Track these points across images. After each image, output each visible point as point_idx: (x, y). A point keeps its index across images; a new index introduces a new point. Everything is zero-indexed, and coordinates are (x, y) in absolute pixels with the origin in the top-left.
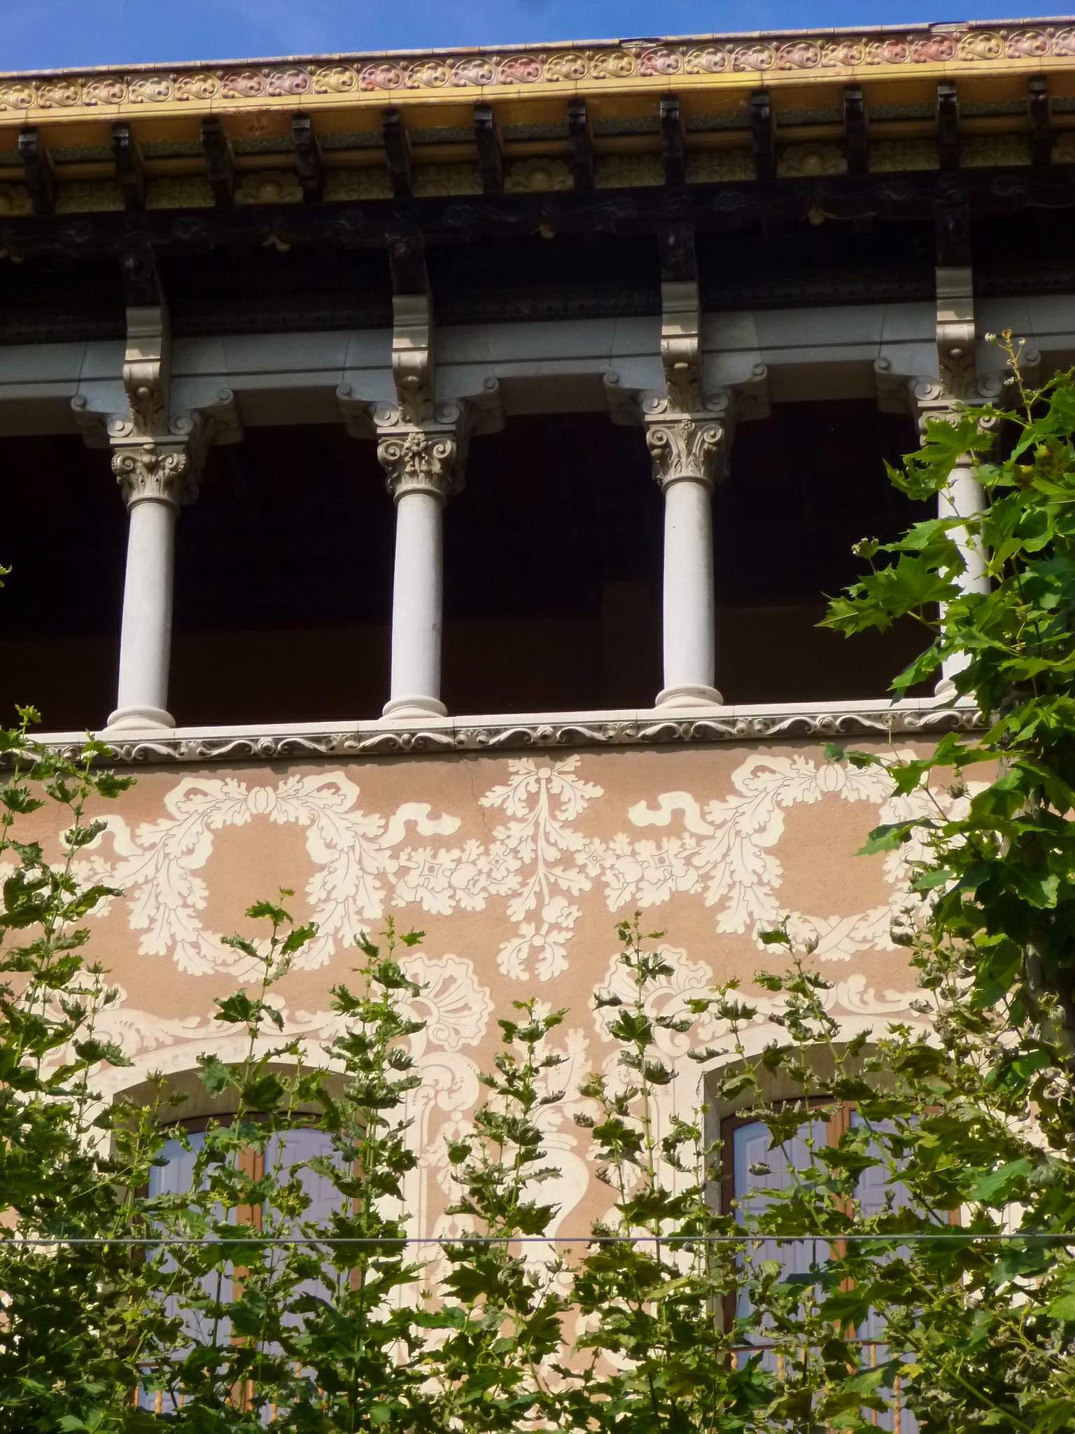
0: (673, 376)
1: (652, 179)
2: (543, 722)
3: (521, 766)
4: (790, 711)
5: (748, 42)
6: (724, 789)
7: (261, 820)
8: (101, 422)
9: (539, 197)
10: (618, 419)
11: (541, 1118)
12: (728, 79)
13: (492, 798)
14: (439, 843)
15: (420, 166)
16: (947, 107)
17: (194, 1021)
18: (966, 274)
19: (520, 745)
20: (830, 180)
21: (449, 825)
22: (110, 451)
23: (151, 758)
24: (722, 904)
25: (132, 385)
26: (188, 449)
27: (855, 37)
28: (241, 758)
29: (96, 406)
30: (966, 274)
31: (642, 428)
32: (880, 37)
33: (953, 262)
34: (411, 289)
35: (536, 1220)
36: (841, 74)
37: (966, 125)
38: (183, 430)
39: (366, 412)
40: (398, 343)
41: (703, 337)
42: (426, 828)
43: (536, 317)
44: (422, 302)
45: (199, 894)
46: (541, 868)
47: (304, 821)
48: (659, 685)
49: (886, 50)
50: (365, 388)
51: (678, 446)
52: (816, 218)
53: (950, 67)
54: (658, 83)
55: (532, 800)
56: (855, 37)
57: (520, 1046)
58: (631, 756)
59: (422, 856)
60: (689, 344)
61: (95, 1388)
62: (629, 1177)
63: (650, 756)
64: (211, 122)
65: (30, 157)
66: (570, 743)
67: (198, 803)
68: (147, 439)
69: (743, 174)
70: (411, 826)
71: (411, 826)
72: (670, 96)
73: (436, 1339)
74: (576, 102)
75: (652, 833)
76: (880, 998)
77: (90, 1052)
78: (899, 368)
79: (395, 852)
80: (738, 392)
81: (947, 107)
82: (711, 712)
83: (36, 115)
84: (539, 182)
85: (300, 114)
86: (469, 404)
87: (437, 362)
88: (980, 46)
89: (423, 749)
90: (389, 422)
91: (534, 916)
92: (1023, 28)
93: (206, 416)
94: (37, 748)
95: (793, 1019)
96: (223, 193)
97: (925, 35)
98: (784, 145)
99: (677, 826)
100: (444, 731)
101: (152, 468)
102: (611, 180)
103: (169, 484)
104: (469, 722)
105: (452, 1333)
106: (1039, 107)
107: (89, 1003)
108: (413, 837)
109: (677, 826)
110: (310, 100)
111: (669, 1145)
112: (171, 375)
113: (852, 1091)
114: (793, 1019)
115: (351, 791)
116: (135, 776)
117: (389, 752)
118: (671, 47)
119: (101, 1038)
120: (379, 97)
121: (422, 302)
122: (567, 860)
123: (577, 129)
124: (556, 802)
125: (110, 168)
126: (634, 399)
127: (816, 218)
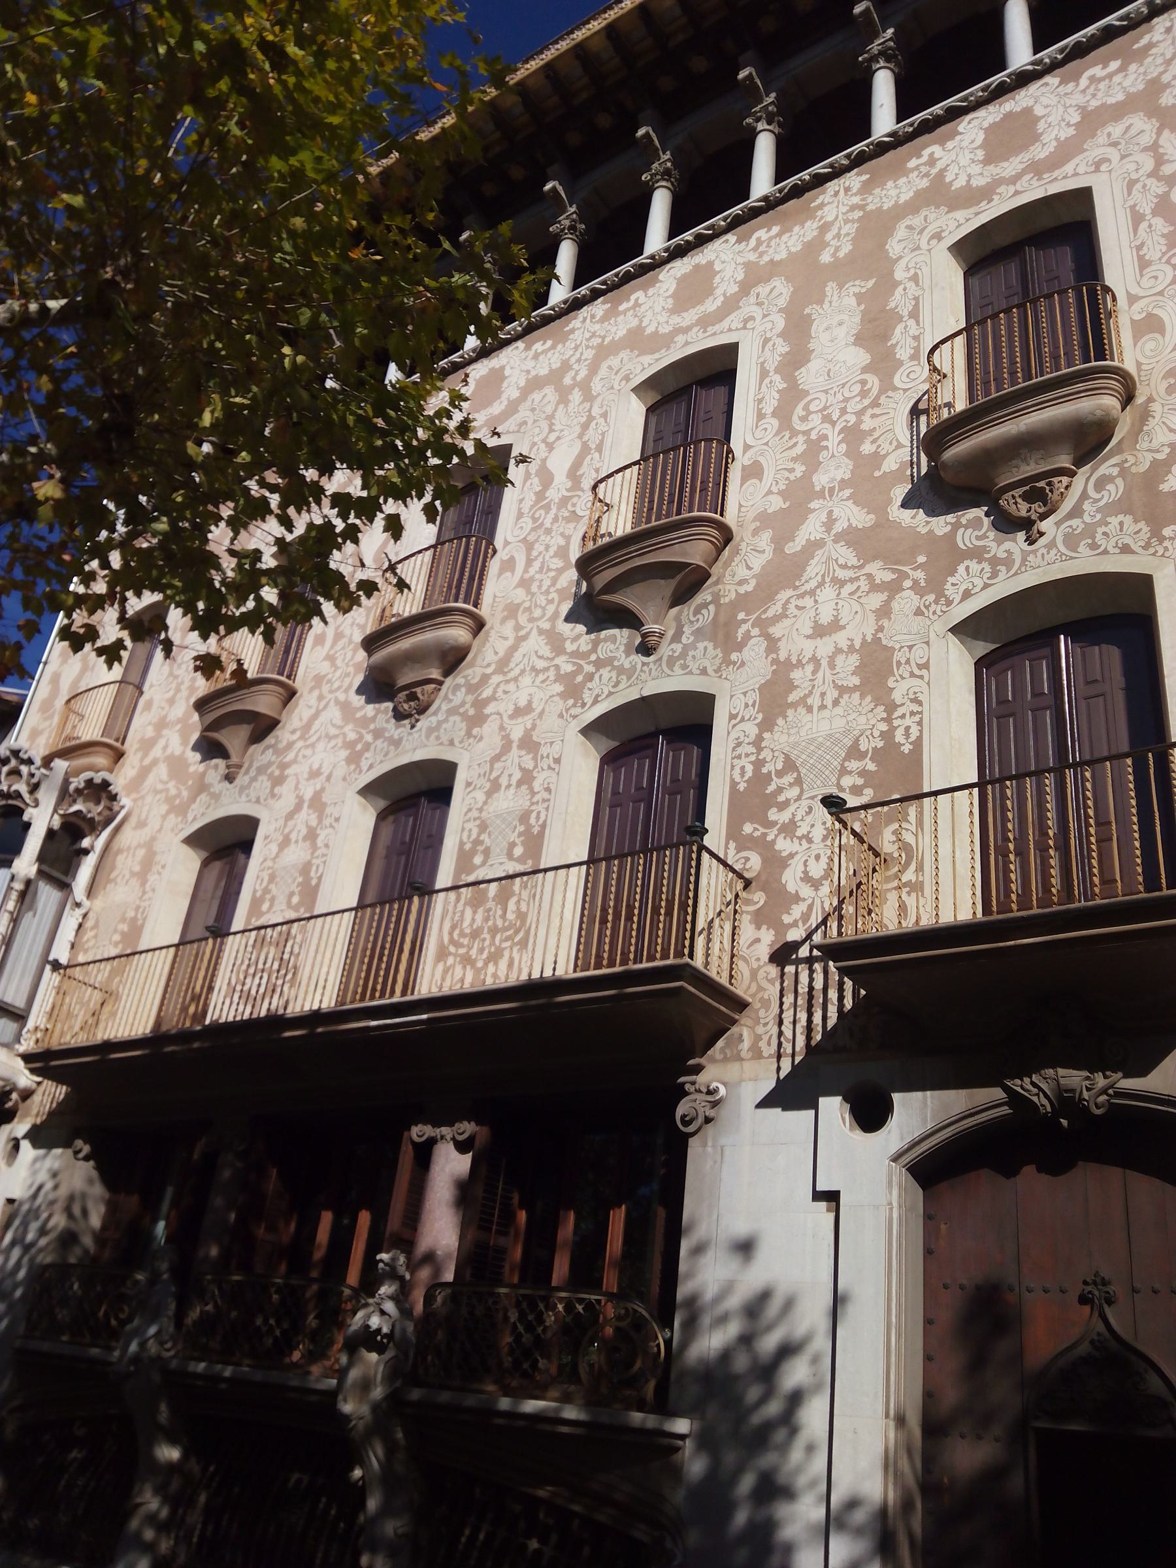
17: (985, 202)
59: (1102, 86)
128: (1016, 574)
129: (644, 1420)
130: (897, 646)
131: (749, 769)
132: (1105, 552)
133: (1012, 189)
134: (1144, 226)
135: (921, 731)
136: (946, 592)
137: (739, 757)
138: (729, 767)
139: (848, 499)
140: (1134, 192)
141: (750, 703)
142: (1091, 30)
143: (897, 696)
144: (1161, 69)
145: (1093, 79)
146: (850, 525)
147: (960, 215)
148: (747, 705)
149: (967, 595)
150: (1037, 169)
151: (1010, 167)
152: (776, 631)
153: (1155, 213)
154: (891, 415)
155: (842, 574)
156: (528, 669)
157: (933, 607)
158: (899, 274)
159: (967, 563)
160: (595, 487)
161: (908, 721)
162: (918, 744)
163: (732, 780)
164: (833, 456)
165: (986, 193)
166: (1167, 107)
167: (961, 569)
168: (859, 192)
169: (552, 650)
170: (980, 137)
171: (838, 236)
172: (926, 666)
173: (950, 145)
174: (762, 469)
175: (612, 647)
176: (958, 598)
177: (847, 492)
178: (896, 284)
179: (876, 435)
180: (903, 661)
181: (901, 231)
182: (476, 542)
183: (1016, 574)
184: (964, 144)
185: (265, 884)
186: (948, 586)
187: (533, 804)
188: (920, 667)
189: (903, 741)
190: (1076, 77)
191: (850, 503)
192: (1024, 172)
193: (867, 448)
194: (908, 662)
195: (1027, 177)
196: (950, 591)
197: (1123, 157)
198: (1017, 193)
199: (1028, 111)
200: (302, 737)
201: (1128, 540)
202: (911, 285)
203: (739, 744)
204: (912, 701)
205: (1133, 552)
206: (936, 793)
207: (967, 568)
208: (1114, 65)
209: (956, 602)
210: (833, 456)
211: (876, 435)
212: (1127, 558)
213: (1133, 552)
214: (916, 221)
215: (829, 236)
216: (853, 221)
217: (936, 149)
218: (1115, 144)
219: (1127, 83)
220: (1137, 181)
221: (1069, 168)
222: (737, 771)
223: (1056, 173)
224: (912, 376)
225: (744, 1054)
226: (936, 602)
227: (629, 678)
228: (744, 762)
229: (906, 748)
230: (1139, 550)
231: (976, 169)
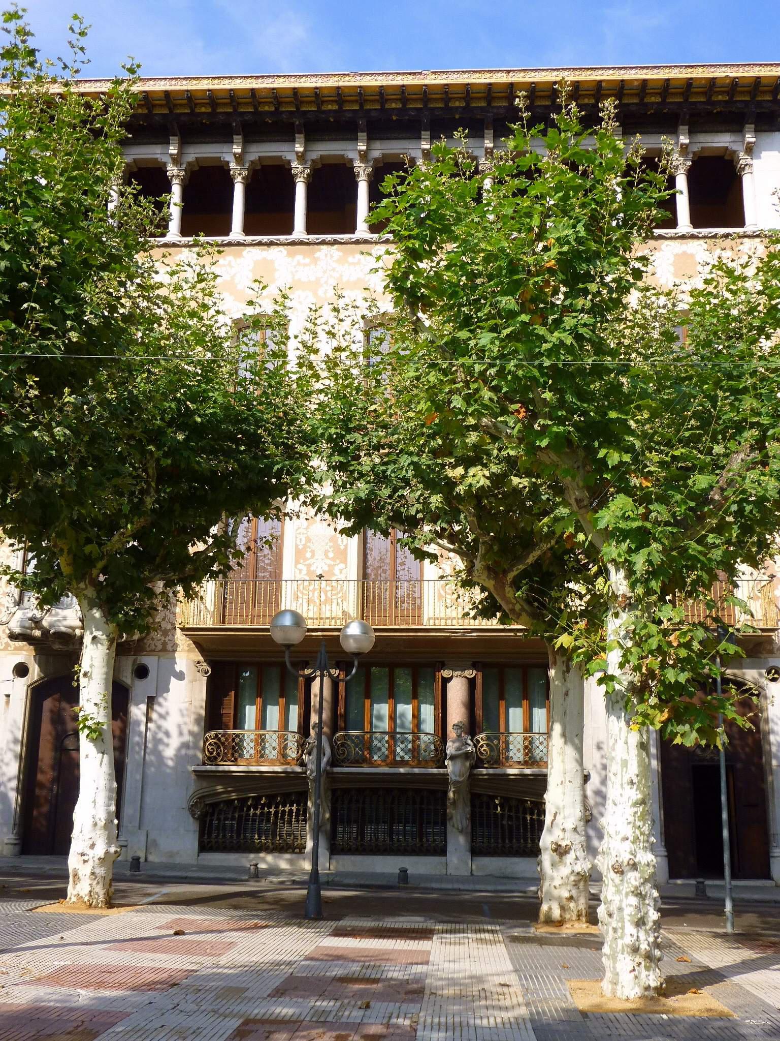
0: (360, 155)
1: (356, 107)
2: (329, 237)
3: (324, 247)
4: (259, 238)
5: (379, 74)
7: (265, 259)
8: (228, 163)
9: (330, 111)
10: (348, 165)
11: (318, 329)
12: (374, 83)
13: (318, 254)
14: (305, 265)
15: (302, 102)
16: (425, 92)
18: (428, 133)
19: (323, 243)
20: (725, 101)
21: (307, 260)
22: (230, 170)
25: (235, 154)
26: (248, 170)
27: (404, 74)
28: (260, 244)
29: (288, 158)
30: (428, 133)
31: (353, 168)
32: (410, 74)
33: (425, 130)
34: (300, 133)
35: (316, 351)
36: (400, 83)
37: (429, 96)
38: (247, 165)
39: (289, 162)
40: (171, 148)
41: (368, 146)
43: (329, 140)
44: (302, 136)
45: (672, 269)
48: (231, 230)
49: (411, 77)
50: (351, 155)
51: (362, 172)
52: (394, 118)
53: (426, 82)
54: (357, 84)
55: (326, 255)
56: (404, 74)
57: (313, 313)
60: (364, 148)
61: (217, 387)
62: (335, 343)
64: (253, 90)
65: (210, 97)
66: (335, 242)
68: (238, 168)
69: (377, 107)
70: (298, 261)
71: (298, 261)
72: (360, 87)
73: (294, 377)
74: (338, 88)
75: (353, 264)
77: (218, 312)
78: (350, 157)
80: (376, 160)
81: (425, 92)
82: (368, 236)
83: (211, 87)
84: (330, 107)
85: (274, 89)
86: (313, 161)
87: (305, 150)
88: (433, 76)
89: (301, 243)
90: (294, 165)
91: (326, 282)
92: (444, 72)
93: (252, 162)
95: (369, 308)
96: (256, 108)
97: (420, 73)
98: (387, 100)
101: (240, 174)
102: (157, 111)
103: (243, 178)
104: (313, 237)
105: (298, 376)
106: (446, 92)
107: (217, 301)
108: (299, 264)
109: (229, 264)
110: (276, 85)
111: (344, 336)
112: (244, 151)
113: (381, 325)
114: (369, 308)
116: (226, 248)
117: (293, 243)
118: (361, 74)
119: (220, 309)
120: (292, 85)
121: (302, 136)
122: (334, 270)
123: (490, 90)
124: (332, 256)
125: (314, 99)
126: (351, 161)
127: (394, 118)
185: (303, 542)
222: (298, 540)
229: (342, 547)
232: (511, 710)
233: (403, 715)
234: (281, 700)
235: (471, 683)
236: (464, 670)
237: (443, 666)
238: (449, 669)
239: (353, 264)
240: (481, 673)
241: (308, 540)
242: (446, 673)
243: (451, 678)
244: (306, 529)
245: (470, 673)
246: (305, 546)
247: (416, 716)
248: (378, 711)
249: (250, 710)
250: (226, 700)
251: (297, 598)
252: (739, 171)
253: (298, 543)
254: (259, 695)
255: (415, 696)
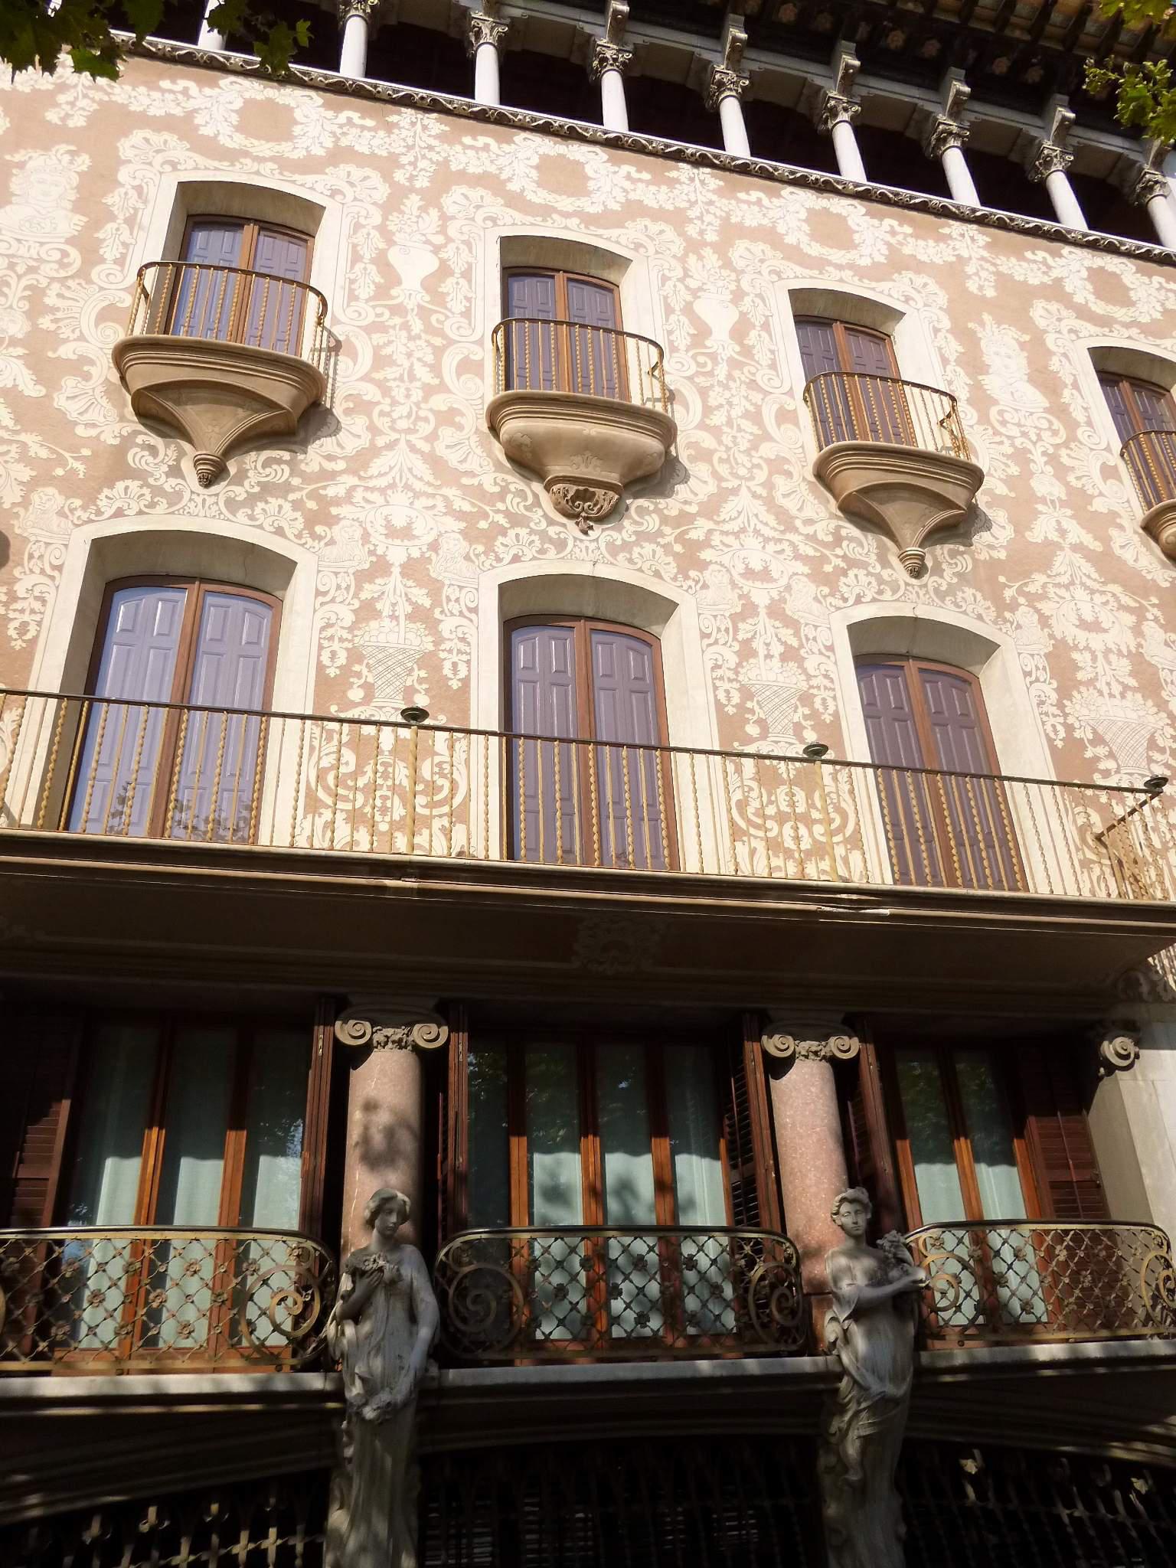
3: (408, 113)
4: (544, 117)
6: (510, 141)
17: (226, 163)
19: (407, 102)
21: (370, 123)
23: (215, 64)
24: (509, 180)
42: (635, 175)
46: (417, 149)
47: (293, 104)
51: (486, 31)
58: (463, 121)
59: (354, 131)
63: (660, 160)
67: (794, 197)
68: (845, 99)
75: (748, 203)
76: (281, 173)
79: (341, 126)
94: (155, 45)
99: (486, 148)
100: (371, 85)
101: (846, 110)
115: (863, 210)
122: (430, 148)
128: (897, 600)
129: (815, 1364)
130: (33, 539)
131: (342, 660)
132: (260, 527)
133: (255, 167)
134: (359, 266)
135: (319, 655)
136: (99, 502)
137: (331, 638)
138: (315, 648)
139: (18, 357)
140: (359, 234)
141: (344, 585)
142: (422, 92)
143: (20, 589)
144: (404, 150)
145: (349, 120)
146: (15, 386)
147: (202, 161)
148: (339, 587)
149: (516, 559)
150: (284, 164)
151: (264, 148)
152: (1046, 607)
153: (373, 261)
154: (81, 304)
155: (418, 486)
156: (400, 485)
157: (79, 513)
158: (123, 175)
159: (128, 482)
160: (661, 355)
161: (26, 617)
162: (466, 682)
163: (319, 663)
164: (11, 307)
165: (232, 156)
166: (49, 122)
167: (120, 486)
168: (436, 137)
169: (17, 421)
170: (238, 104)
171: (72, 104)
172: (59, 568)
173: (207, 91)
174: (776, 417)
175: (150, 459)
176: (508, 558)
177: (20, 351)
178: (117, 184)
179: (59, 315)
180: (36, 555)
181: (138, 136)
182: (826, 382)
183: (897, 600)
184: (221, 99)
186: (102, 496)
187: (812, 687)
188: (470, 610)
189: (450, 675)
190: (338, 109)
191: (20, 362)
192: (272, 159)
193: (45, 323)
194: (41, 557)
195: (270, 165)
196: (102, 503)
197: (355, 199)
198: (258, 173)
199: (288, 109)
200: (354, 472)
201: (981, 611)
202: (133, 194)
203: (329, 626)
204: (37, 598)
205: (286, 537)
206: (284, 716)
207: (127, 488)
208: (646, 176)
209: (106, 515)
210: (11, 307)
211: (59, 315)
212: (979, 623)
213: (286, 537)
214: (157, 139)
215: (62, 98)
216: (93, 100)
217: (192, 85)
218: (352, 184)
219: (375, 143)
220: (364, 226)
221: (309, 179)
223: (296, 177)
224: (111, 278)
225: (1145, 996)
226: (84, 508)
227: (170, 505)
228: (336, 645)
229: (455, 684)
230: (292, 537)
231: (228, 130)
232: (186, 1164)
233: (626, 1187)
234: (231, 1136)
235: (845, 1075)
236: (825, 1037)
237: (339, 1008)
238: (360, 1017)
239: (748, 203)
240: (871, 1047)
241: (747, 693)
242: (349, 1032)
243: (366, 1050)
244: (350, 629)
245: (428, 1034)
246: (346, 671)
247: (665, 1185)
248: (553, 1175)
249: (116, 1173)
250: (34, 1135)
251: (736, 834)
252: (1139, 196)
253: (325, 659)
254: (158, 1116)
255: (659, 1126)
